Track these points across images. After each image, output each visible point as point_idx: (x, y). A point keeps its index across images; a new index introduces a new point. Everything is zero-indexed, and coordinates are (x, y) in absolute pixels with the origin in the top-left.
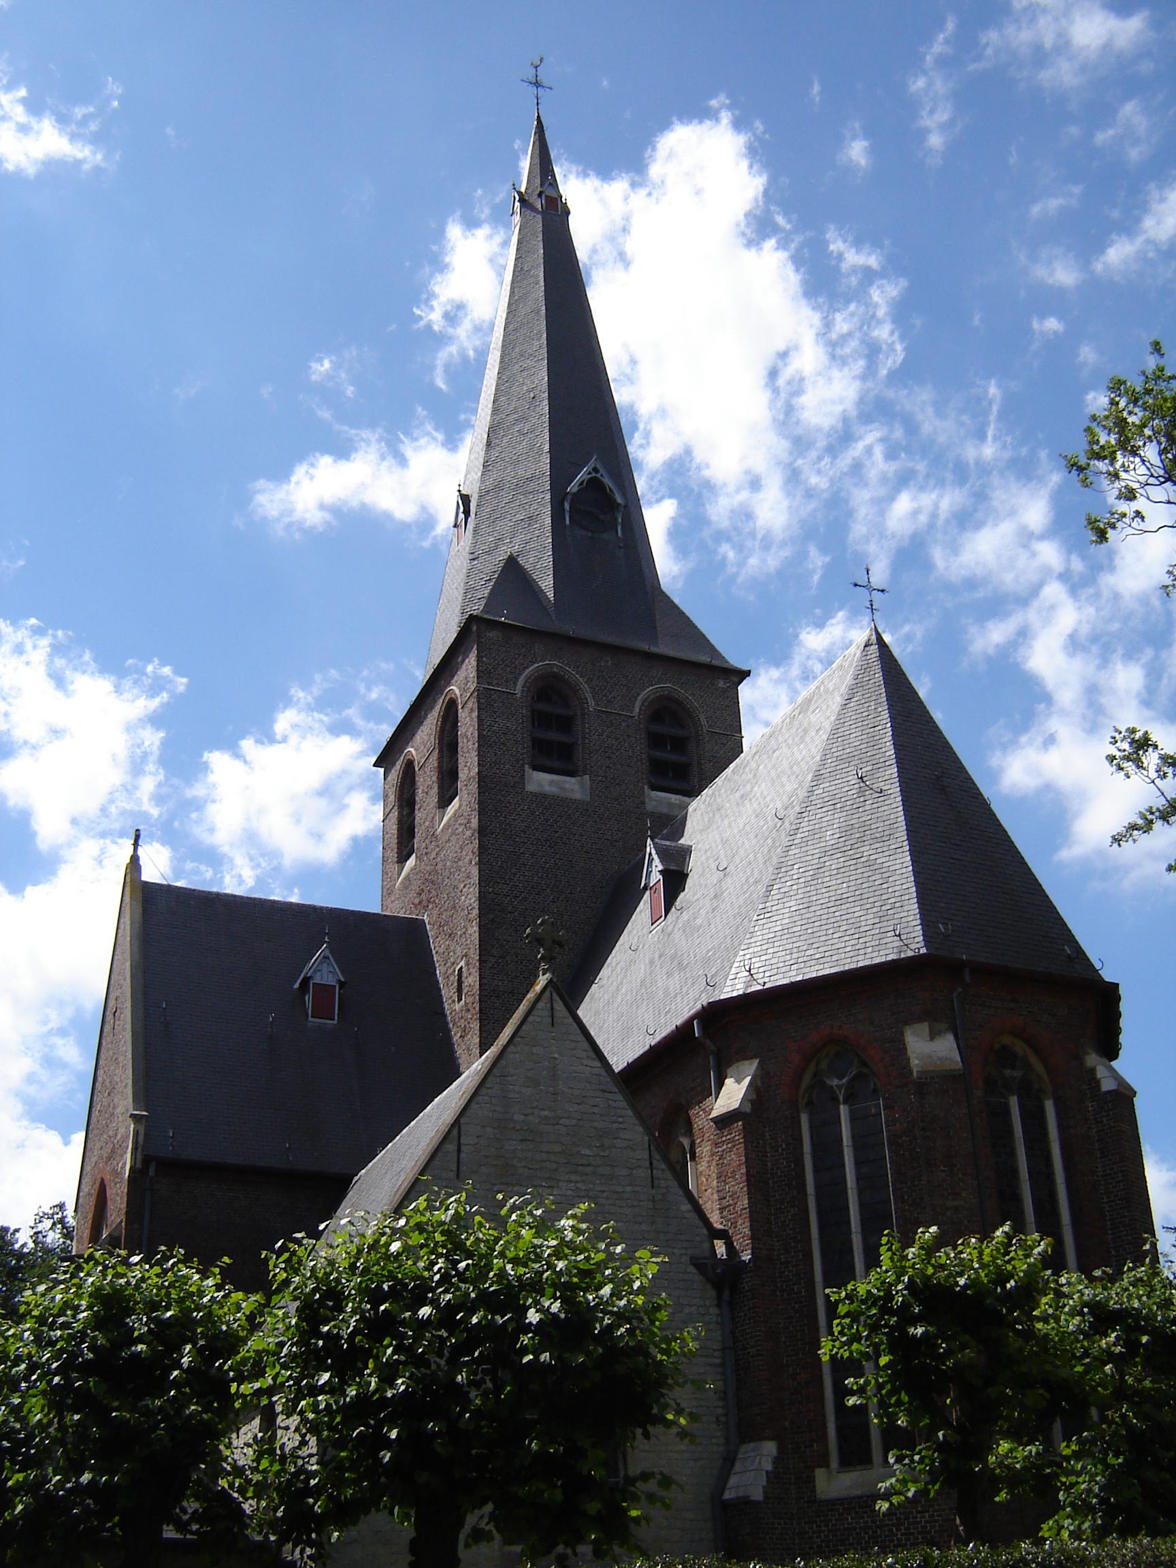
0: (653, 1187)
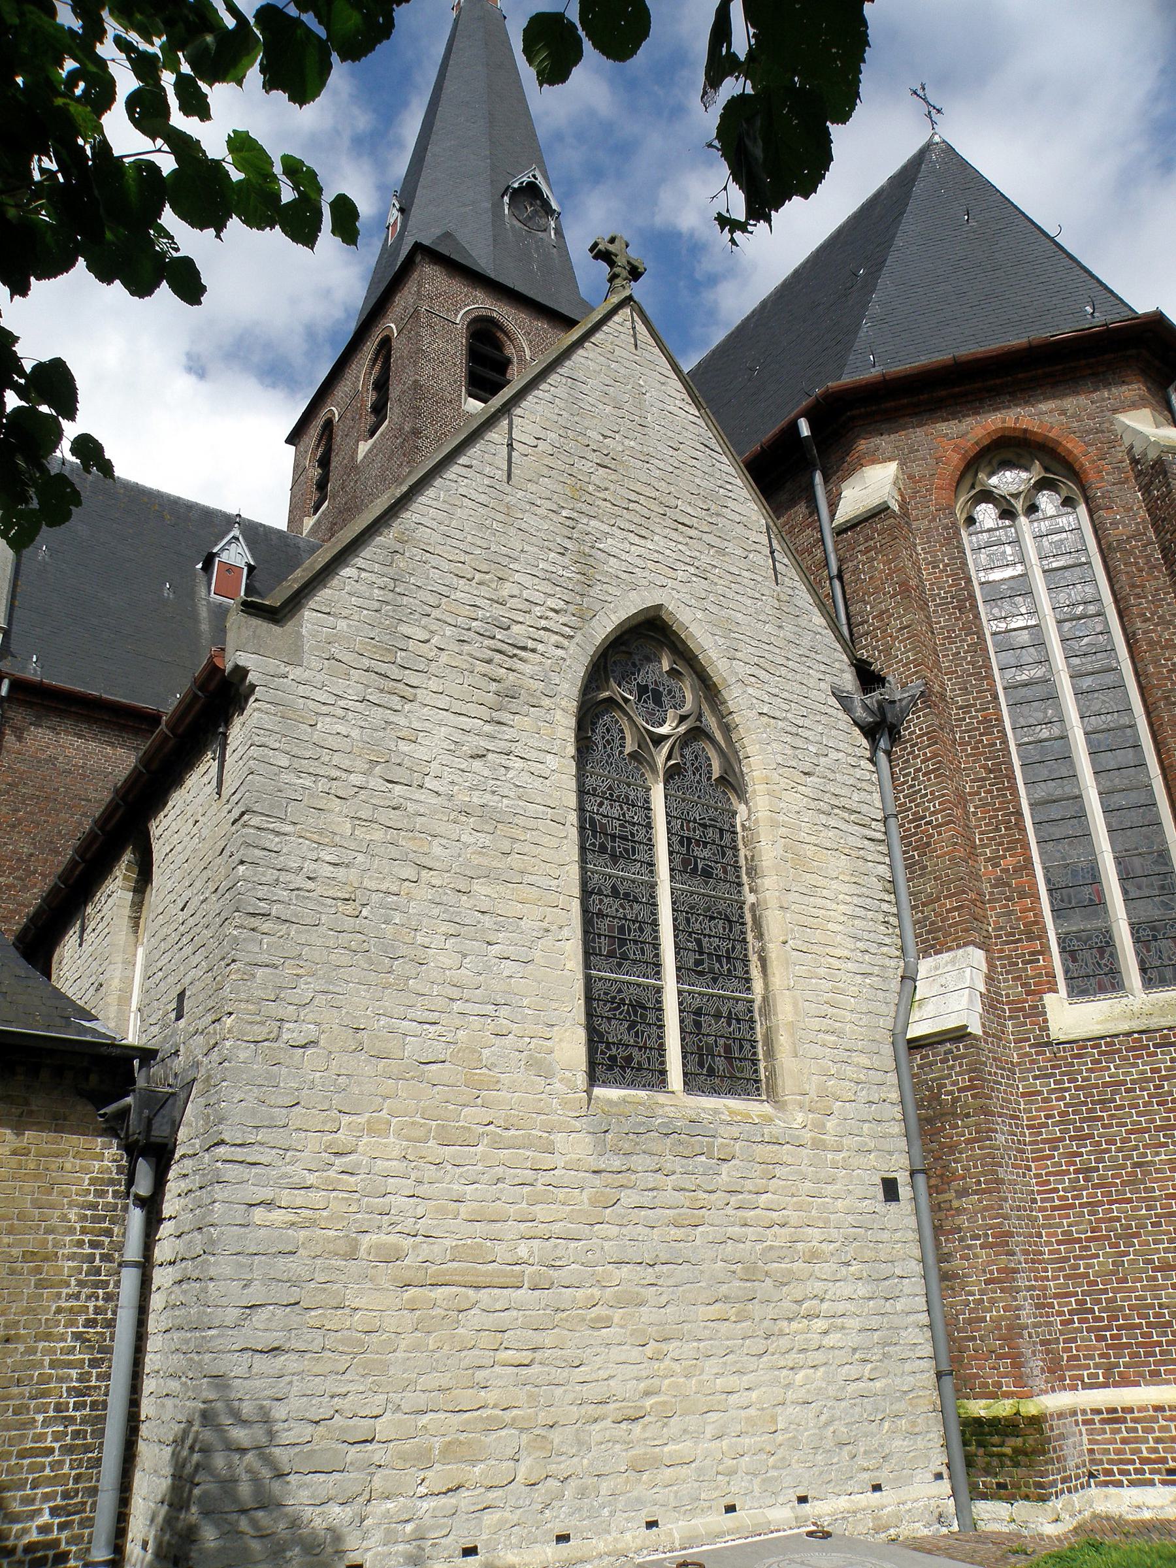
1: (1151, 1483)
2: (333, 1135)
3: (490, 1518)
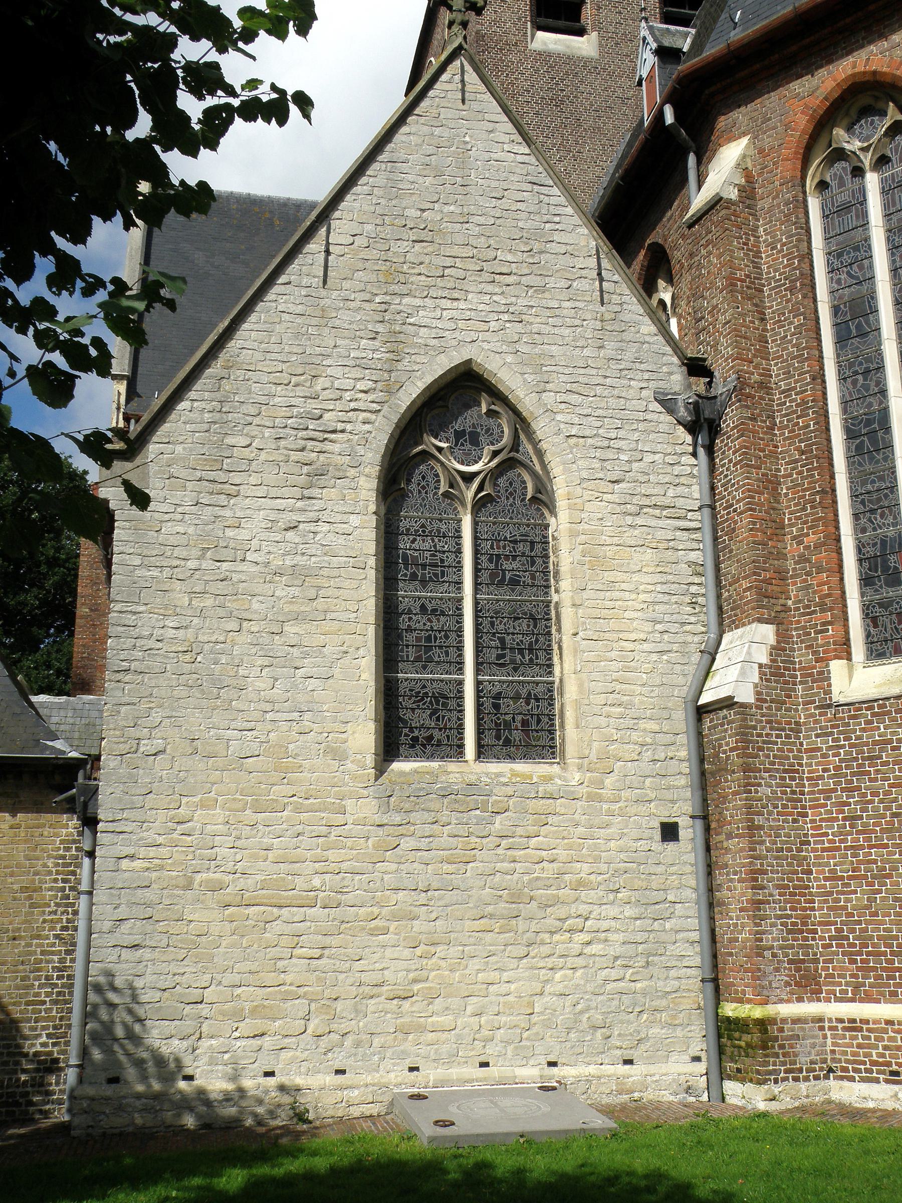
0: (602, 304)
1: (877, 1081)
2: (176, 811)
3: (285, 1055)
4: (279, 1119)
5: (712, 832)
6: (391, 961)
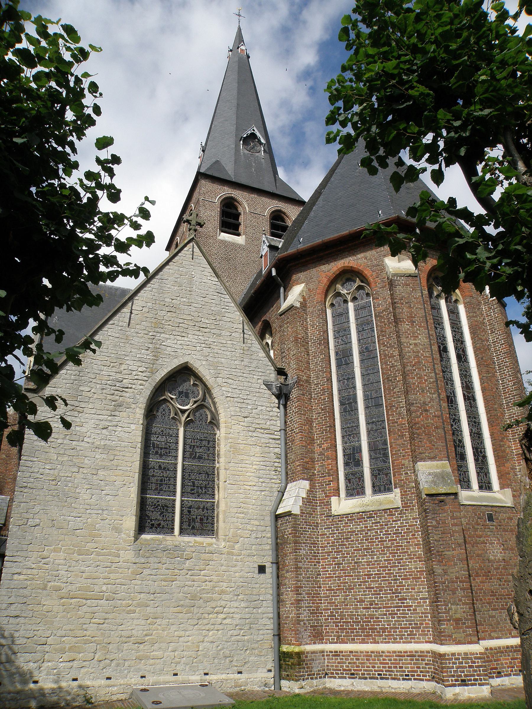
0: (193, 259)
1: (345, 678)
3: (83, 670)
4: (78, 702)
5: (280, 570)
6: (136, 626)
